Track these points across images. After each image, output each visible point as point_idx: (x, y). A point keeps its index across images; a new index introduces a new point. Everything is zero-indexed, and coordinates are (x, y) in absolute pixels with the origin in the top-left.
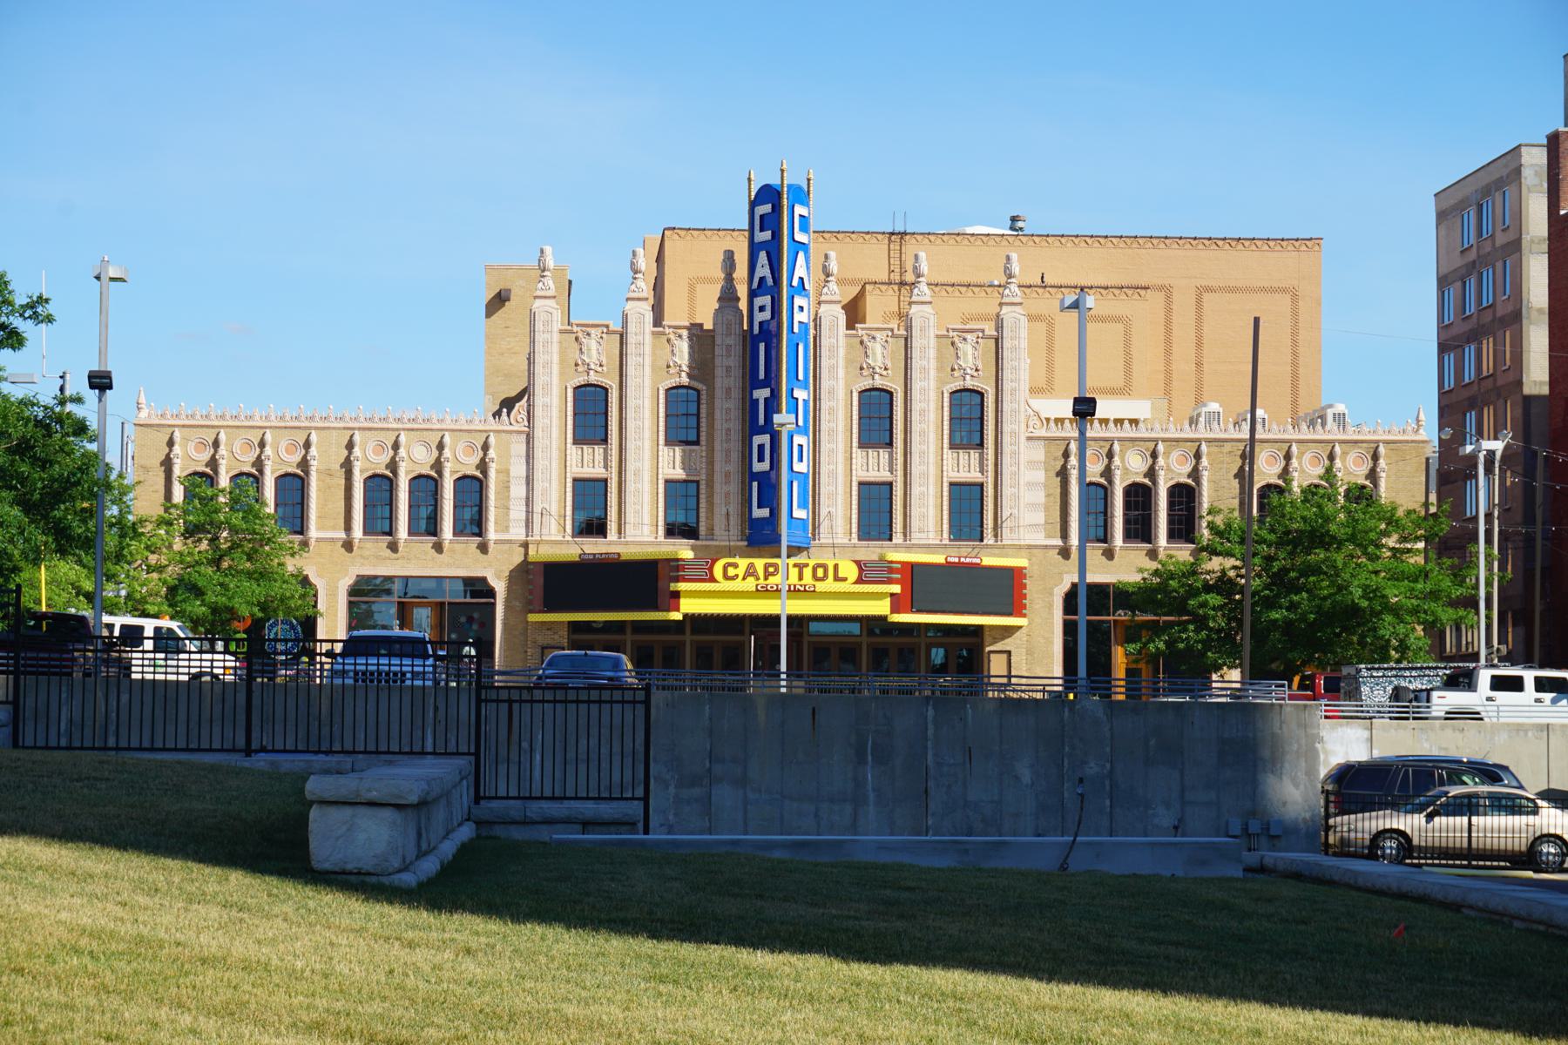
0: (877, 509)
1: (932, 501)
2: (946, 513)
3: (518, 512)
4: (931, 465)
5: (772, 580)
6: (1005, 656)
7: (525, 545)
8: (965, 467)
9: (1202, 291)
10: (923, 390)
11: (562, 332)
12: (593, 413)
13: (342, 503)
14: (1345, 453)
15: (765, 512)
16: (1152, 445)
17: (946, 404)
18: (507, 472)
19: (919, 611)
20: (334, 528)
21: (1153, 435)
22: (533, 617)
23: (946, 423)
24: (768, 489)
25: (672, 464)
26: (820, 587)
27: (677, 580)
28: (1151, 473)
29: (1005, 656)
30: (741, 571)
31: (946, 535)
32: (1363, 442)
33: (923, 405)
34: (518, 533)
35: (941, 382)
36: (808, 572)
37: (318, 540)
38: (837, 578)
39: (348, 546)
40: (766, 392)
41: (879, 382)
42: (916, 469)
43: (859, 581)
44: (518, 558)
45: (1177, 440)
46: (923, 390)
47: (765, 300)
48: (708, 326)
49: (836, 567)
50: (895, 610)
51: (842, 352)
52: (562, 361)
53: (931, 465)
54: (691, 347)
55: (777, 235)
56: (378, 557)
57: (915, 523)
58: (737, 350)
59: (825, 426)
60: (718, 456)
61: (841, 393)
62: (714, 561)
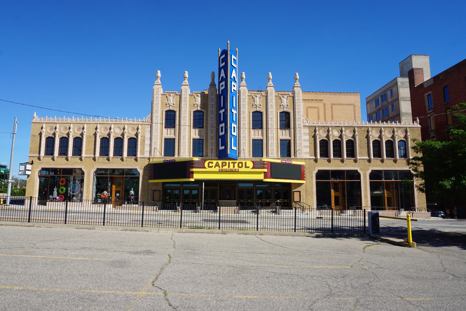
0: (258, 147)
1: (275, 145)
2: (279, 149)
3: (147, 148)
4: (274, 135)
5: (224, 168)
6: (299, 193)
7: (149, 159)
8: (285, 135)
9: (332, 105)
10: (271, 112)
11: (162, 95)
12: (171, 119)
13: (93, 146)
14: (397, 131)
15: (223, 148)
16: (340, 128)
17: (279, 116)
18: (144, 136)
19: (273, 178)
20: (90, 154)
21: (341, 125)
22: (150, 181)
23: (279, 121)
24: (224, 140)
25: (195, 134)
26: (240, 170)
27: (193, 168)
28: (341, 136)
29: (299, 193)
30: (214, 164)
31: (279, 155)
32: (402, 127)
33: (272, 116)
34: (147, 155)
35: (277, 109)
36: (236, 165)
37: (85, 157)
38: (246, 167)
39: (94, 159)
40: (223, 110)
41: (258, 109)
42: (270, 135)
43: (253, 168)
44: (147, 163)
45: (348, 127)
46: (271, 112)
47: (223, 83)
48: (206, 92)
49: (246, 163)
50: (265, 177)
51: (247, 100)
52: (162, 103)
53: (274, 135)
54: (201, 99)
55: (226, 64)
56: (103, 163)
57: (270, 152)
58: (215, 100)
59: (242, 122)
60: (209, 131)
61: (247, 112)
62: (205, 161)
